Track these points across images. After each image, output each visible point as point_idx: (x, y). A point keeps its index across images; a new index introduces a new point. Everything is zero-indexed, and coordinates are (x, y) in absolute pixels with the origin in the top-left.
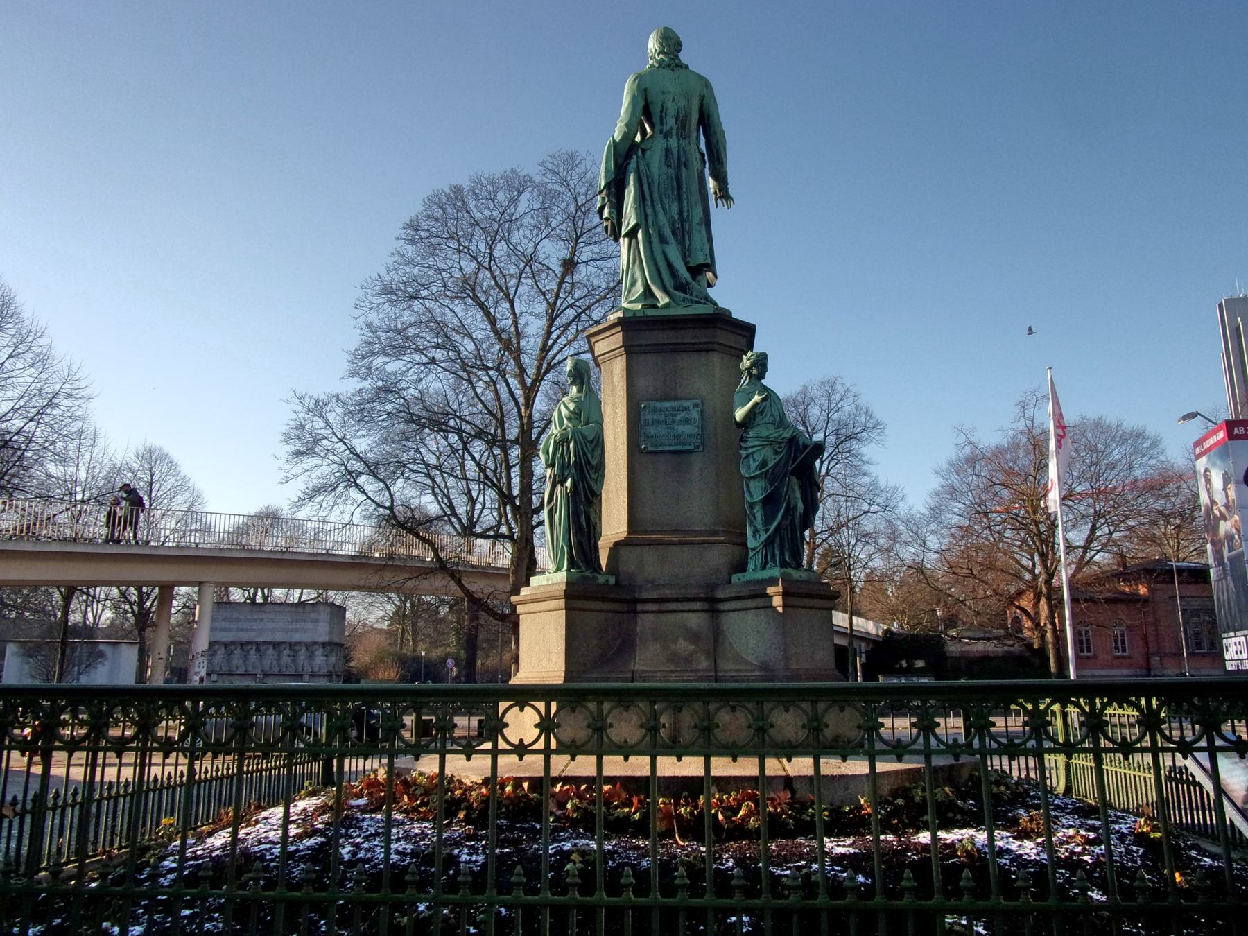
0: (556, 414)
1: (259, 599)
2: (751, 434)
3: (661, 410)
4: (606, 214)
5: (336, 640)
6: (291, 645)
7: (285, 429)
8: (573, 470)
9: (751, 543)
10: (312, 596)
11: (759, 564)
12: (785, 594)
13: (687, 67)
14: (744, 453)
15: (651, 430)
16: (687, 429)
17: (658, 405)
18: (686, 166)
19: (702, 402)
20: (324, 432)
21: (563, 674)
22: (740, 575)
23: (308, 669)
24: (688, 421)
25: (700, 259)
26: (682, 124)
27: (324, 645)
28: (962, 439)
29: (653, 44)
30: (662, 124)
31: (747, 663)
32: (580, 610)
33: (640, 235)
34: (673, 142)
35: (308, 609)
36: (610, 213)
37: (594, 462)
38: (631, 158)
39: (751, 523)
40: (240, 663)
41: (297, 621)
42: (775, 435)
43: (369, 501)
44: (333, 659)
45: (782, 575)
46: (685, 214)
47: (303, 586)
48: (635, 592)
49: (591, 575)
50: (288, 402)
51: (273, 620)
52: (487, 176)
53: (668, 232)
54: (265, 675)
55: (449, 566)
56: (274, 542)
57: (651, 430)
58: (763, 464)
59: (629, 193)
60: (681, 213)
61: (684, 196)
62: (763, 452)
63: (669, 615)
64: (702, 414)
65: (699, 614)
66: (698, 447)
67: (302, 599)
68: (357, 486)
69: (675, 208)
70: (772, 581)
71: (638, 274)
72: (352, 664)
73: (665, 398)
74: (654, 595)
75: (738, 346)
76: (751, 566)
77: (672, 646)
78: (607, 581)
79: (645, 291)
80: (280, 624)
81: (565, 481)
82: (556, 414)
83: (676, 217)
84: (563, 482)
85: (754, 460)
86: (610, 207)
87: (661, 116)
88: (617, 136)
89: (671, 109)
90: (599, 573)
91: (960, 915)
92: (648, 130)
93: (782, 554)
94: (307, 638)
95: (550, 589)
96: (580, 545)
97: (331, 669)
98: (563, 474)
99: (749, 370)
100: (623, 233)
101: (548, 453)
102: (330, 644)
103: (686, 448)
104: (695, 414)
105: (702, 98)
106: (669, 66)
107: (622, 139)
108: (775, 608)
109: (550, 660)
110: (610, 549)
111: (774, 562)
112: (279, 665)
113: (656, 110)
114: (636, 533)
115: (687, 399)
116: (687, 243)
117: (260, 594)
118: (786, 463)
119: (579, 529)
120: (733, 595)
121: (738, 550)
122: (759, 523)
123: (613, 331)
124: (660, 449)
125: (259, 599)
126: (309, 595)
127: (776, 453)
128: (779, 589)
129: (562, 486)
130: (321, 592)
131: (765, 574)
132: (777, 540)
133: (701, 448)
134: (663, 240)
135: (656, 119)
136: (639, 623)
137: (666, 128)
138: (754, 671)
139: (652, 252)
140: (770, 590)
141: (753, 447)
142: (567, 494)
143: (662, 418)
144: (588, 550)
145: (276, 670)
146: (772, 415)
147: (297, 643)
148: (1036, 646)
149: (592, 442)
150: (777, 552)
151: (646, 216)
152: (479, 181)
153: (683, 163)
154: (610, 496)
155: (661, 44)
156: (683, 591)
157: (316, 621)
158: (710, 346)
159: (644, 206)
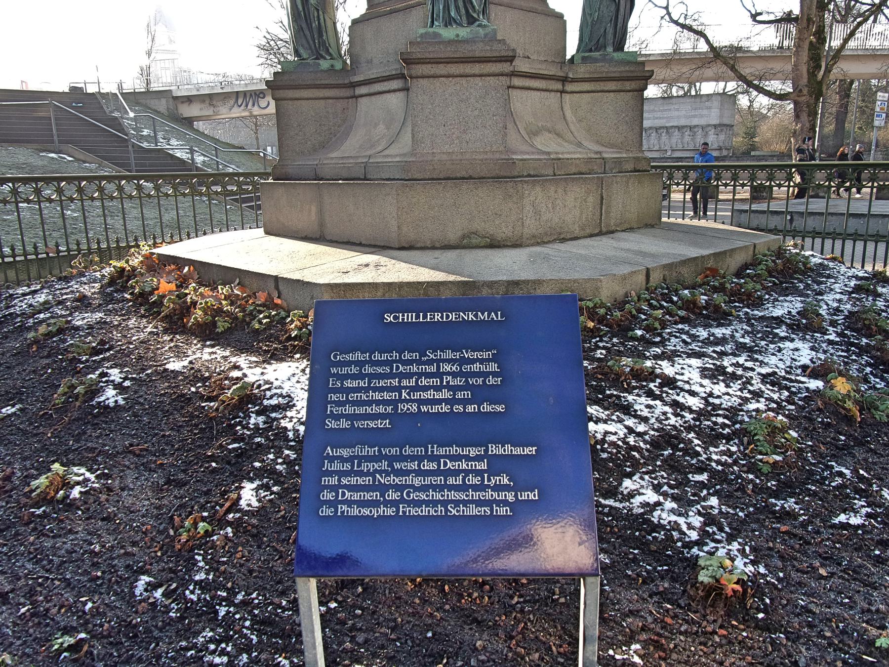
6: (691, 128)
27: (715, 126)
32: (291, 99)
35: (704, 99)
40: (656, 142)
44: (722, 137)
51: (678, 110)
55: (722, 53)
65: (398, 93)
72: (756, 139)
78: (332, 66)
80: (684, 112)
91: (532, 491)
94: (703, 122)
97: (721, 144)
102: (720, 125)
145: (680, 147)
147: (695, 126)
157: (710, 108)
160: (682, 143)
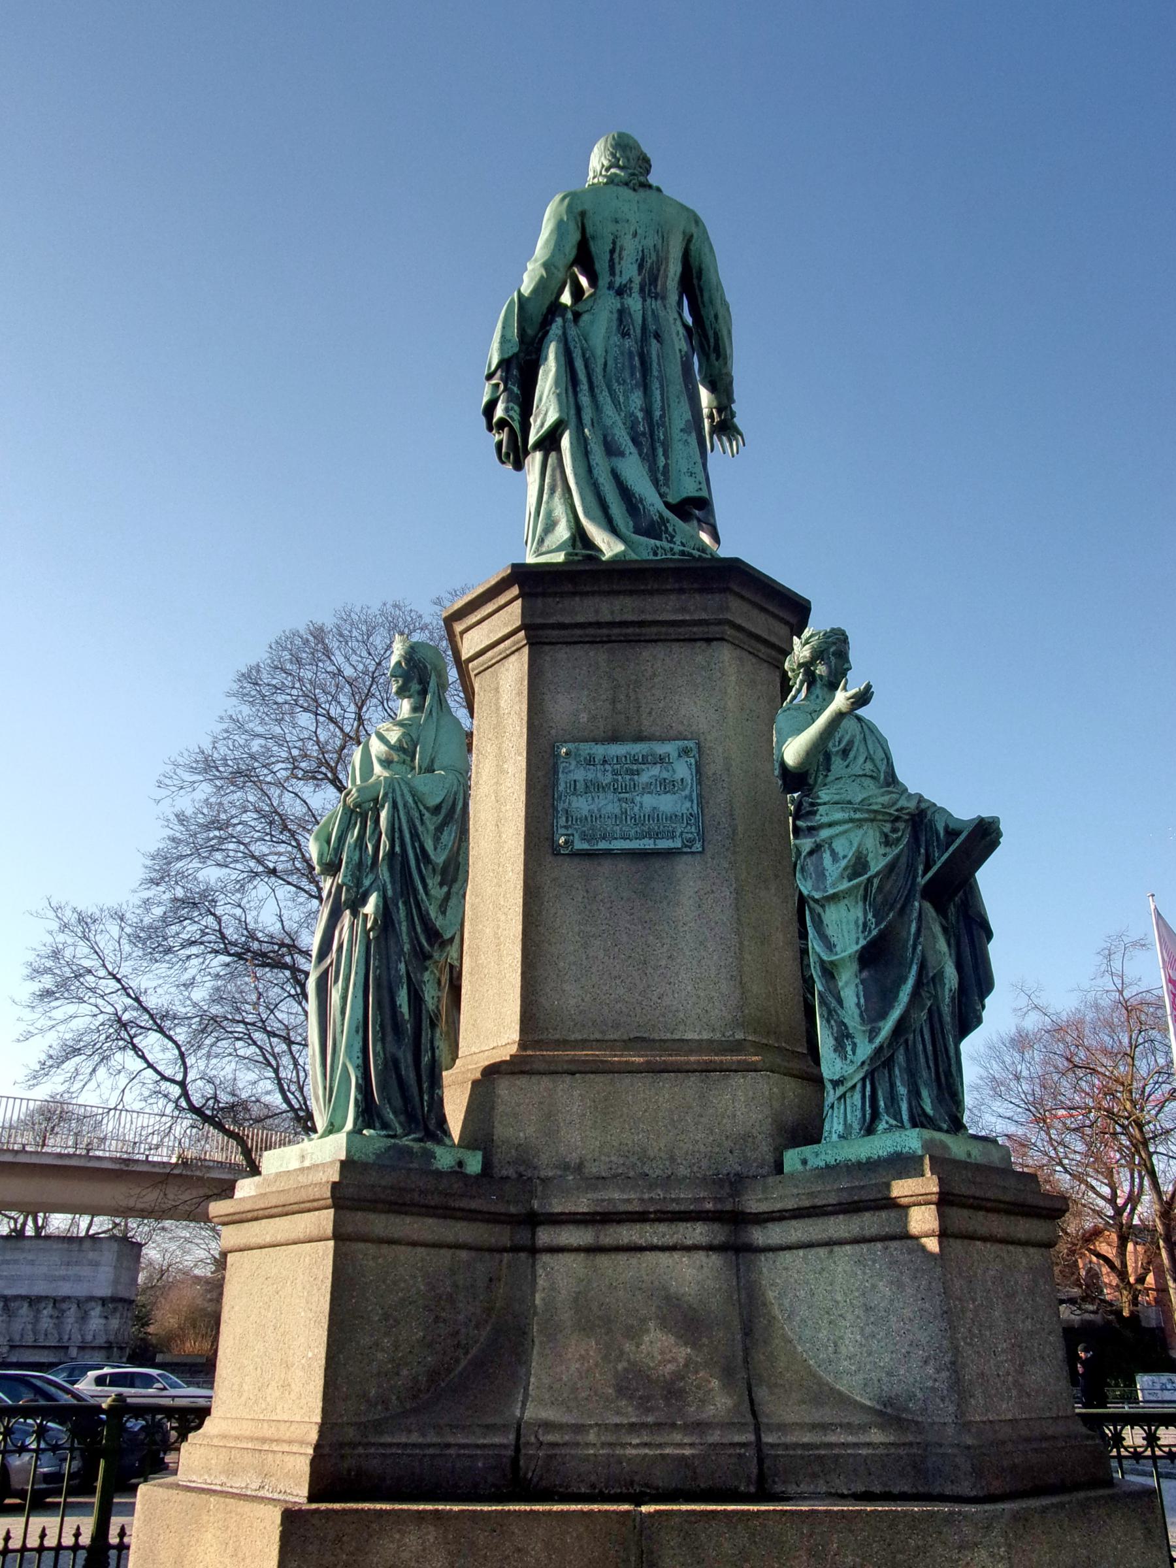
0: (357, 754)
1: (30, 1231)
2: (824, 795)
3: (605, 762)
4: (499, 413)
5: (123, 1293)
6: (56, 1301)
7: (31, 957)
8: (384, 873)
9: (831, 1066)
10: (105, 1228)
11: (854, 1118)
12: (945, 1201)
13: (659, 190)
14: (807, 844)
15: (581, 805)
16: (667, 803)
17: (600, 750)
18: (657, 336)
19: (698, 744)
20: (87, 963)
21: (314, 1436)
22: (807, 1151)
23: (76, 1338)
24: (667, 786)
25: (689, 488)
26: (651, 286)
27: (103, 1301)
28: (1023, 1002)
29: (598, 160)
30: (612, 272)
31: (843, 1400)
33: (565, 442)
34: (634, 303)
36: (507, 410)
37: (439, 858)
38: (552, 321)
39: (830, 1015)
41: (68, 1264)
42: (881, 800)
43: (150, 1071)
44: (115, 1323)
45: (928, 1145)
46: (657, 413)
47: (94, 1212)
48: (532, 1194)
49: (416, 1146)
50: (38, 915)
51: (32, 1263)
52: (358, 609)
53: (622, 437)
54: (12, 1347)
56: (59, 1144)
57: (581, 805)
58: (859, 865)
59: (546, 373)
60: (648, 412)
61: (655, 386)
62: (856, 836)
63: (622, 1258)
64: (698, 771)
65: (700, 1256)
66: (691, 841)
67: (91, 1232)
68: (135, 1048)
69: (636, 400)
70: (904, 1164)
71: (560, 511)
72: (151, 1329)
73: (614, 738)
74: (583, 1204)
75: (773, 639)
76: (834, 1125)
77: (628, 1347)
78: (460, 1164)
79: (573, 539)
80: (44, 1269)
81: (363, 901)
82: (357, 754)
83: (640, 415)
84: (356, 905)
85: (834, 854)
86: (508, 401)
87: (612, 260)
88: (527, 288)
89: (630, 249)
90: (440, 1142)
92: (584, 281)
93: (915, 1094)
95: (303, 1179)
96: (391, 1065)
97: (112, 1338)
98: (359, 884)
99: (807, 667)
100: (532, 439)
101: (328, 842)
102: (114, 1299)
103: (663, 844)
104: (682, 770)
105: (689, 240)
106: (627, 184)
107: (535, 291)
108: (916, 1238)
109: (285, 1386)
110: (475, 1083)
111: (897, 1116)
112: (35, 1334)
113: (602, 250)
114: (538, 1044)
115: (662, 740)
116: (661, 461)
117: (30, 1222)
118: (911, 868)
119: (391, 1024)
120: (790, 1204)
121: (792, 1089)
122: (851, 1013)
123: (502, 600)
124: (603, 845)
125: (30, 1231)
126: (102, 1224)
127: (887, 842)
128: (928, 1184)
129: (355, 914)
130: (117, 1220)
131: (881, 1145)
132: (901, 1057)
133: (697, 847)
134: (611, 450)
135: (601, 266)
136: (541, 1282)
137: (618, 281)
138: (864, 1428)
139: (590, 470)
140: (901, 1189)
141: (830, 825)
142: (366, 933)
143: (608, 779)
144: (415, 1090)
145: (29, 1340)
146: (869, 758)
148: (1126, 1313)
149: (437, 810)
150: (902, 1090)
151: (579, 410)
152: (347, 617)
153: (651, 333)
154: (482, 959)
155: (613, 155)
156: (659, 1193)
157: (96, 1264)
158: (714, 630)
159: (576, 393)
160: (35, 1332)
